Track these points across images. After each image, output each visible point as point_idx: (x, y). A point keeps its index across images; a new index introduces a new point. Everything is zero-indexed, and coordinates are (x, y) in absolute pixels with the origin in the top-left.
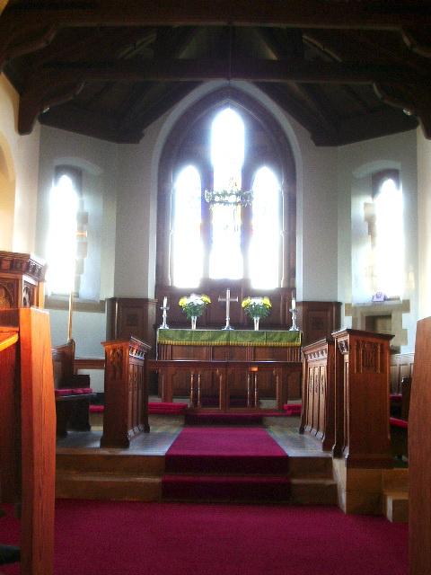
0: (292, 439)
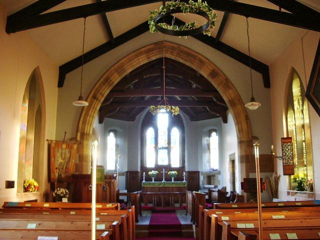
0: (182, 217)
